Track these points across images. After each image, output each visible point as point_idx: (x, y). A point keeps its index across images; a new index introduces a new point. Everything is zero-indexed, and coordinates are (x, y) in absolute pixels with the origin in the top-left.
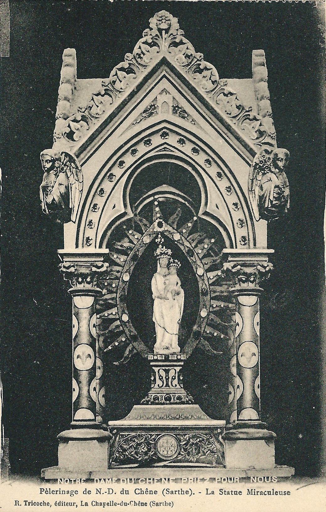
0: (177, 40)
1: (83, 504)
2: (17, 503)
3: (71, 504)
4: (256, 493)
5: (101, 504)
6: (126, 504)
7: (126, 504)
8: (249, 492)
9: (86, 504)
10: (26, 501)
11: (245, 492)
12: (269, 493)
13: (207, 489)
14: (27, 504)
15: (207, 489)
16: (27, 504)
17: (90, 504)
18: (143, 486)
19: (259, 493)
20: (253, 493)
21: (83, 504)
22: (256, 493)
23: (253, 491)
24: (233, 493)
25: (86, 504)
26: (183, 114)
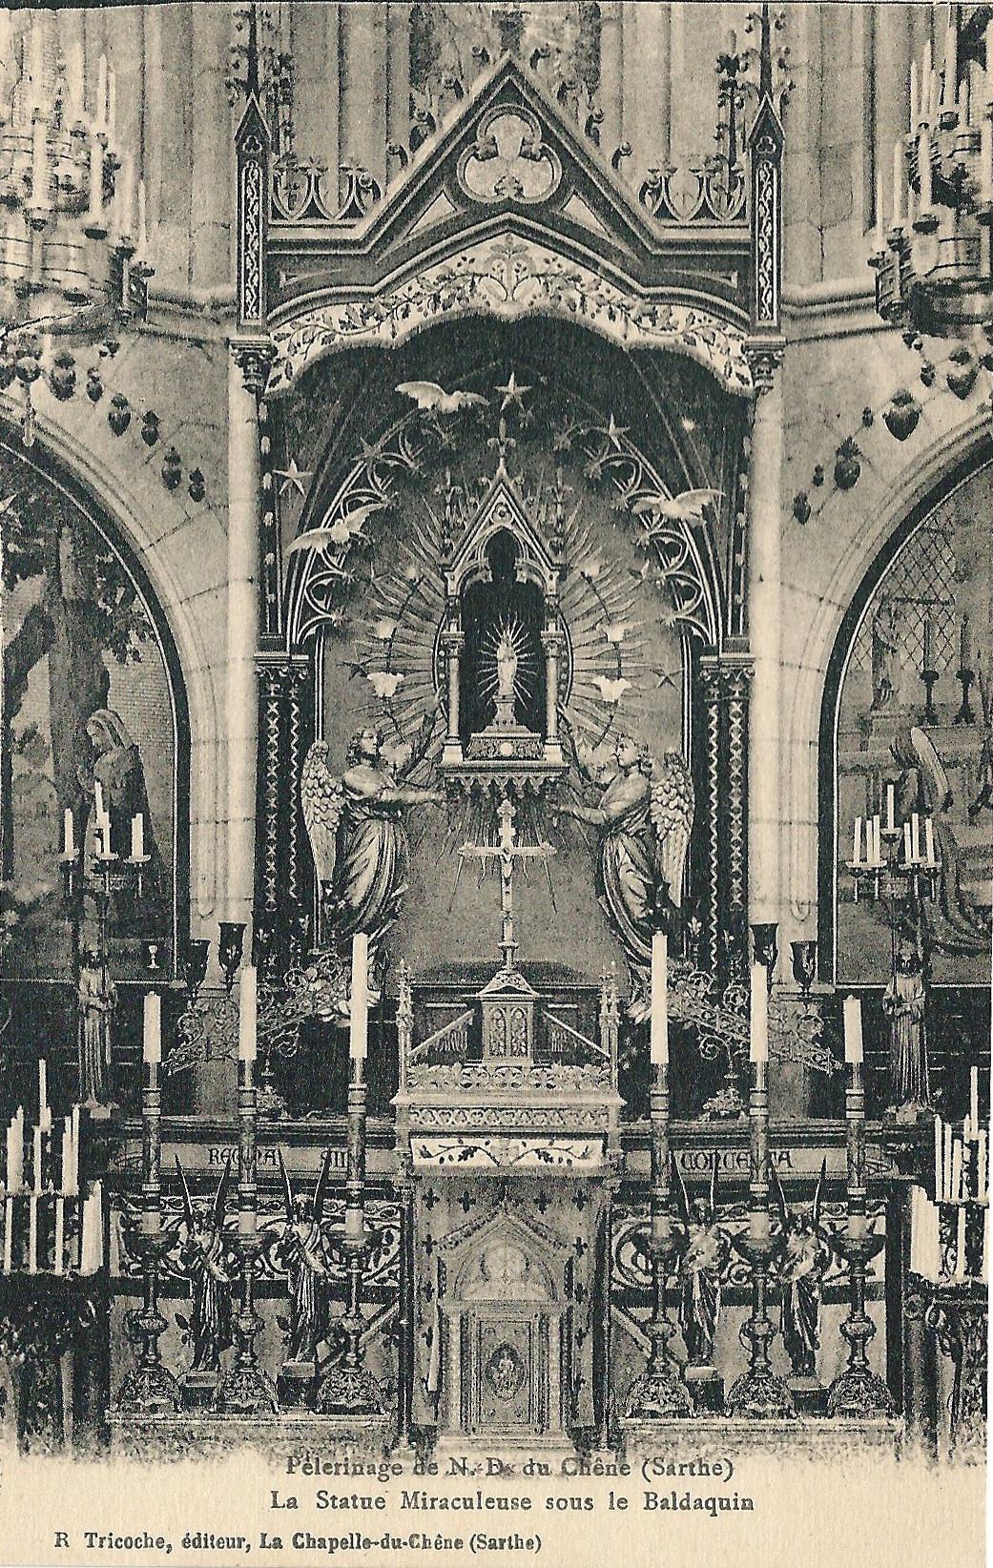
0: (967, 142)
1: (269, 1541)
2: (61, 1539)
3: (516, 1543)
4: (429, 1504)
5: (322, 1543)
6: (397, 1544)
7: (397, 1544)
8: (651, 1500)
9: (278, 1543)
10: (92, 1535)
11: (601, 1502)
12: (468, 1504)
13: (275, 1494)
14: (96, 1541)
15: (275, 1494)
16: (96, 1541)
17: (287, 1542)
18: (341, 1485)
19: (437, 1504)
20: (420, 1504)
21: (269, 1541)
22: (429, 1504)
23: (420, 1496)
24: (359, 1502)
25: (278, 1543)
26: (190, 483)
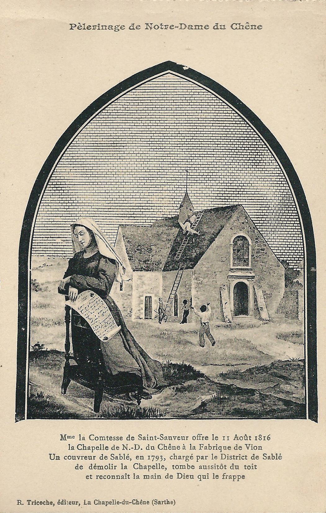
2: (19, 502)
17: (92, 503)
